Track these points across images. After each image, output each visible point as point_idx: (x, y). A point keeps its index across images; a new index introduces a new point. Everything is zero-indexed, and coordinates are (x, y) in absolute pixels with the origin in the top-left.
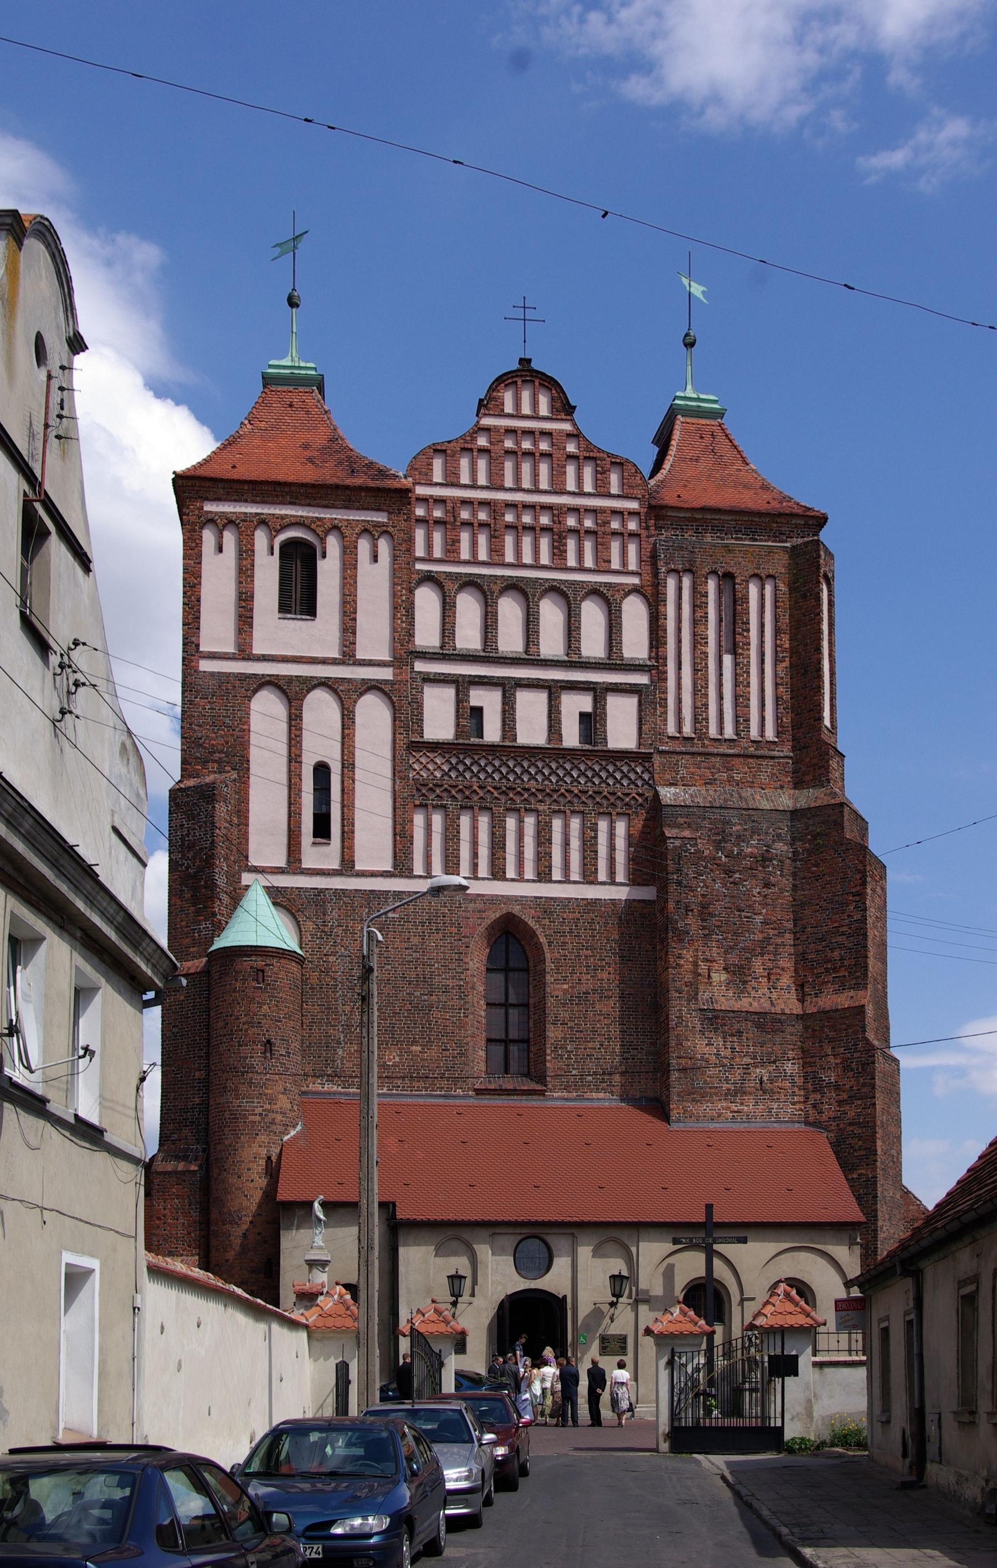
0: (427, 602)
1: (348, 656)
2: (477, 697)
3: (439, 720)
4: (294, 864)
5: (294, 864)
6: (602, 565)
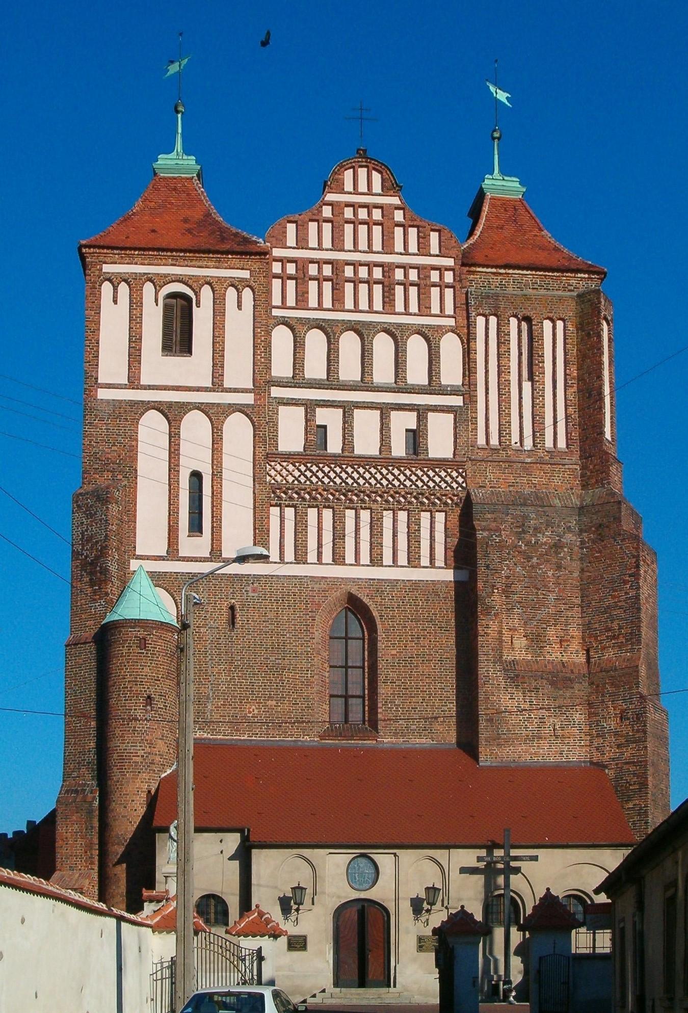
0: (282, 338)
1: (217, 385)
3: (291, 434)
4: (173, 552)
5: (173, 552)
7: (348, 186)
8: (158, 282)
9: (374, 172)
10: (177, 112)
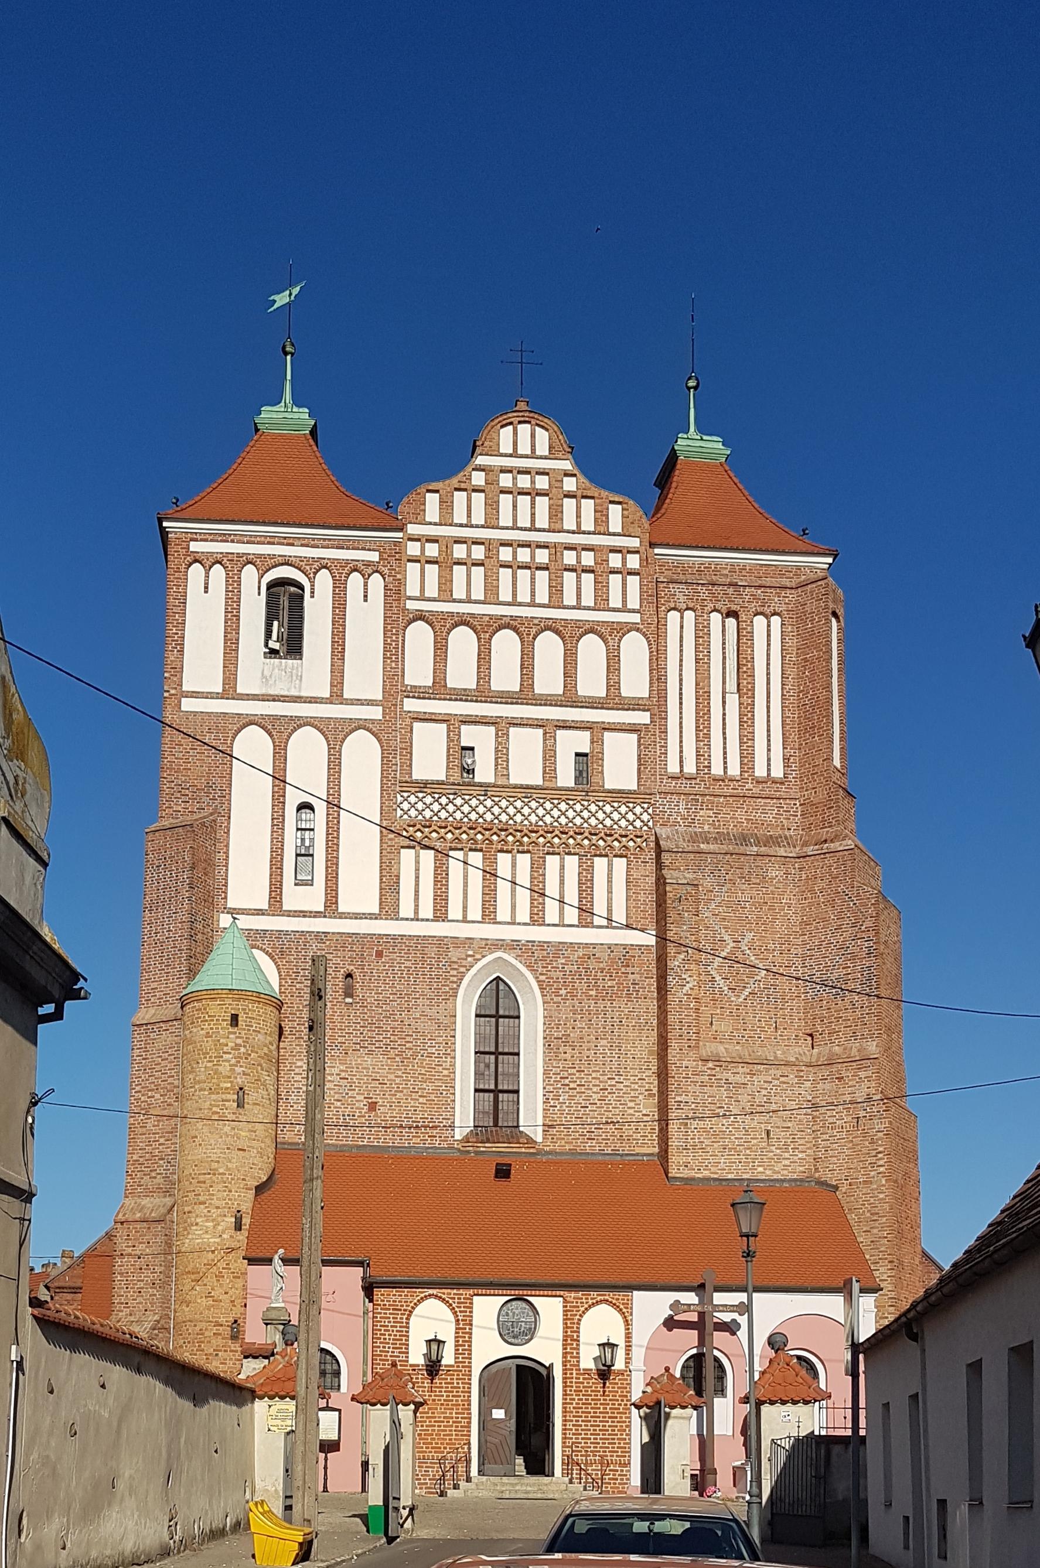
0: (419, 639)
1: (337, 696)
2: (469, 735)
3: (429, 757)
4: (276, 904)
5: (276, 904)
6: (602, 602)
7: (506, 447)
8: (263, 564)
9: (537, 428)
10: (286, 353)
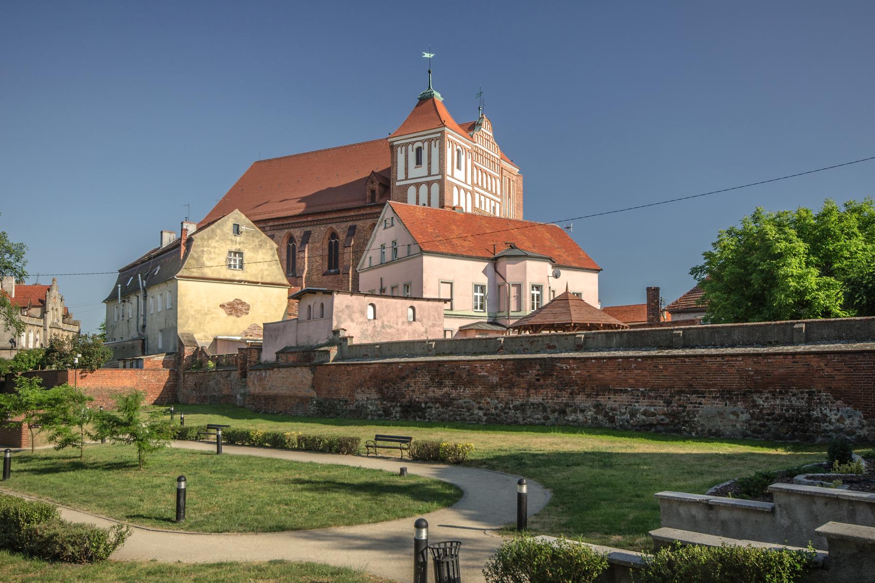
8: (413, 143)
